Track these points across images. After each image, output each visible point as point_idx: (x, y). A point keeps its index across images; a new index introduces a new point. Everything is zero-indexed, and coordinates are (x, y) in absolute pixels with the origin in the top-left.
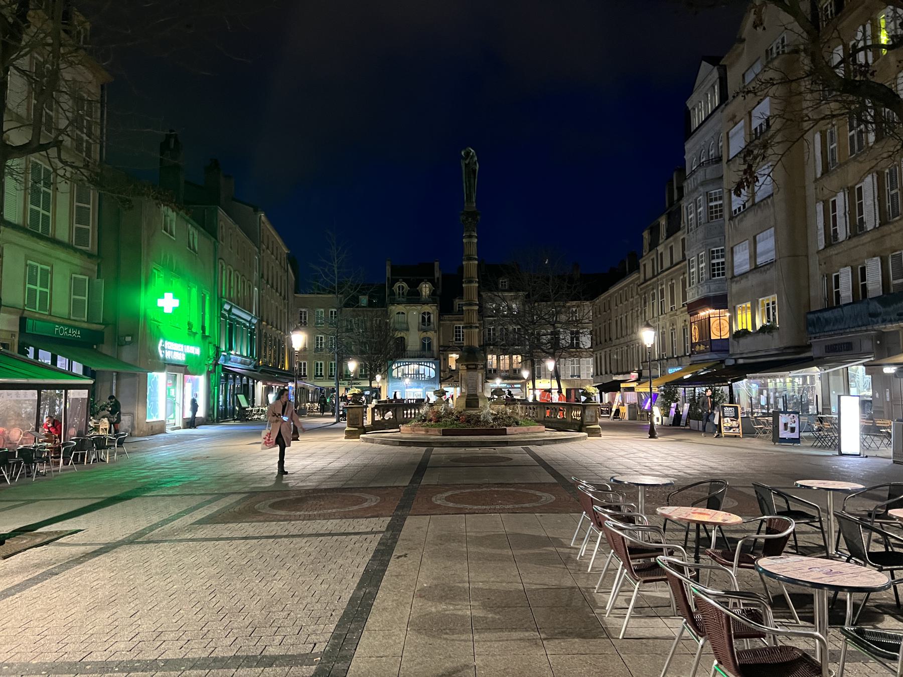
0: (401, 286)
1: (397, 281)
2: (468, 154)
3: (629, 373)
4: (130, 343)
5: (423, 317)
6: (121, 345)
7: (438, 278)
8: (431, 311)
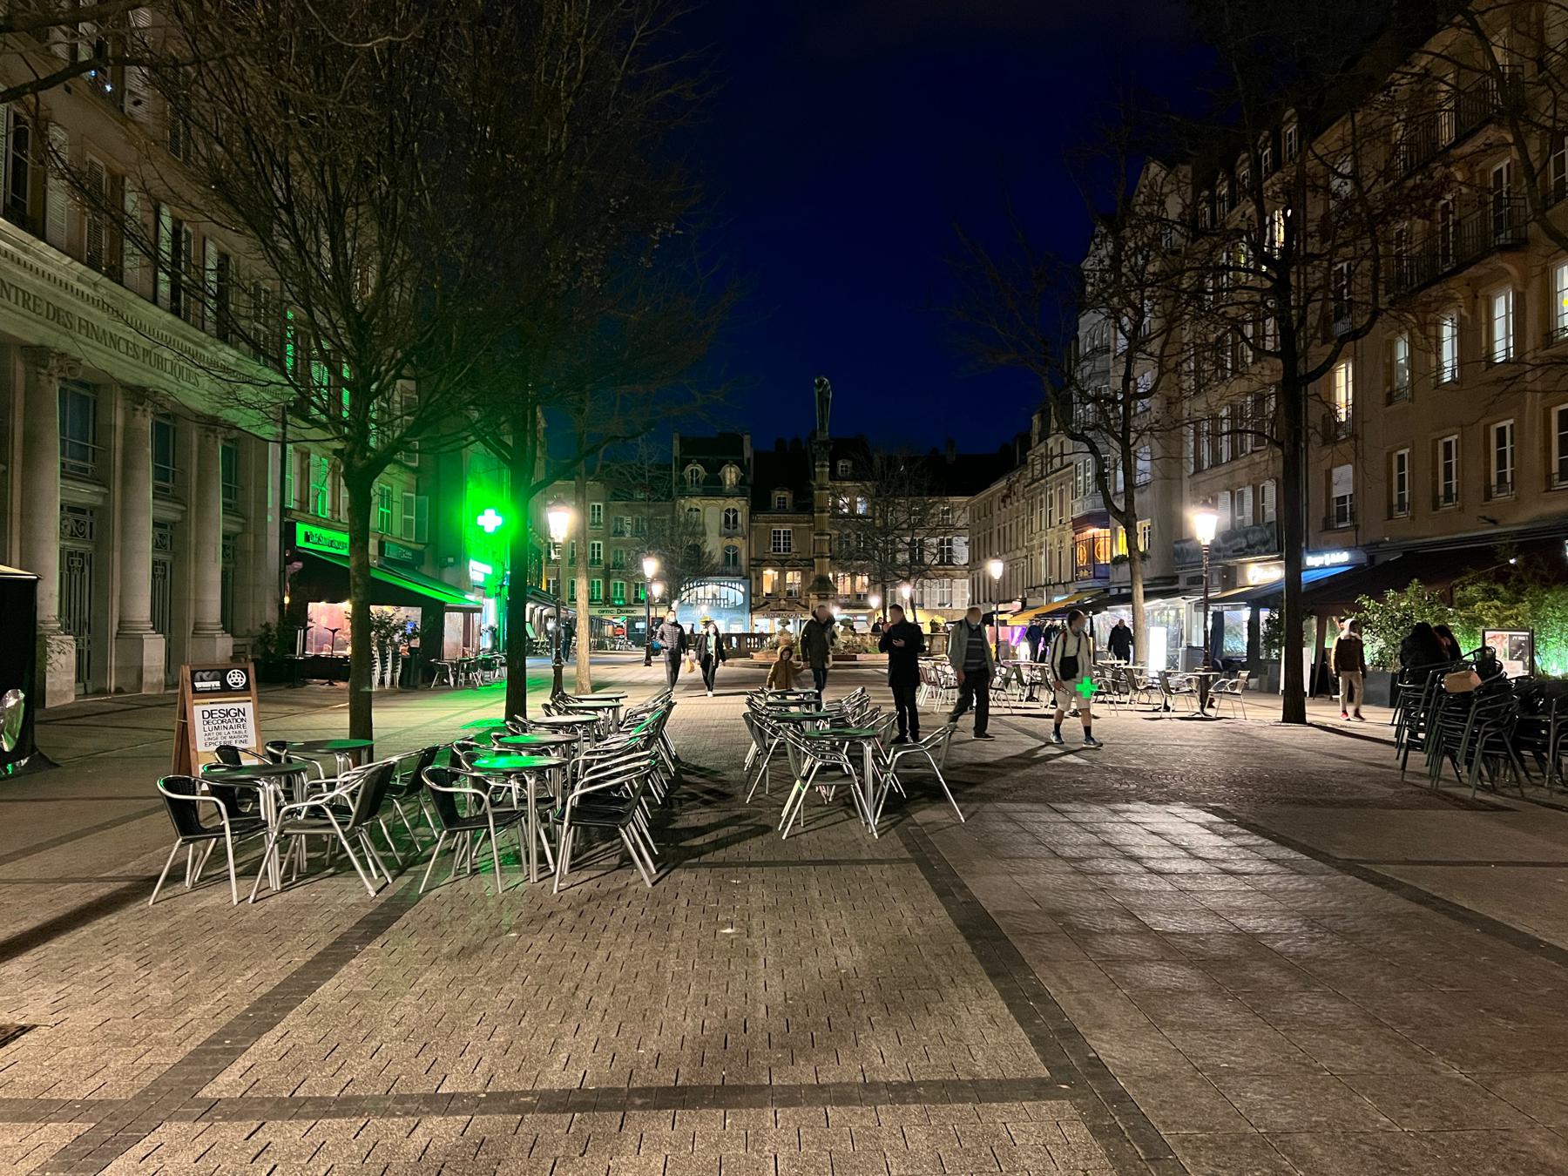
0: (696, 469)
1: (689, 462)
2: (821, 382)
3: (1010, 601)
4: (452, 565)
5: (726, 516)
6: (443, 567)
7: (749, 460)
8: (737, 508)
